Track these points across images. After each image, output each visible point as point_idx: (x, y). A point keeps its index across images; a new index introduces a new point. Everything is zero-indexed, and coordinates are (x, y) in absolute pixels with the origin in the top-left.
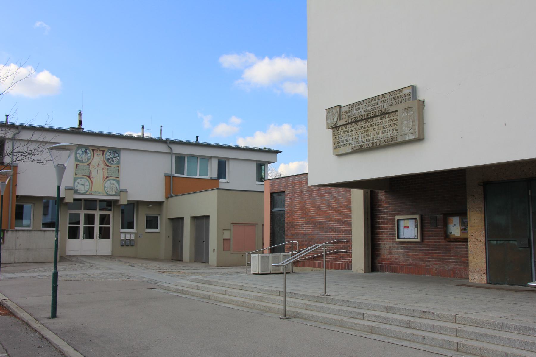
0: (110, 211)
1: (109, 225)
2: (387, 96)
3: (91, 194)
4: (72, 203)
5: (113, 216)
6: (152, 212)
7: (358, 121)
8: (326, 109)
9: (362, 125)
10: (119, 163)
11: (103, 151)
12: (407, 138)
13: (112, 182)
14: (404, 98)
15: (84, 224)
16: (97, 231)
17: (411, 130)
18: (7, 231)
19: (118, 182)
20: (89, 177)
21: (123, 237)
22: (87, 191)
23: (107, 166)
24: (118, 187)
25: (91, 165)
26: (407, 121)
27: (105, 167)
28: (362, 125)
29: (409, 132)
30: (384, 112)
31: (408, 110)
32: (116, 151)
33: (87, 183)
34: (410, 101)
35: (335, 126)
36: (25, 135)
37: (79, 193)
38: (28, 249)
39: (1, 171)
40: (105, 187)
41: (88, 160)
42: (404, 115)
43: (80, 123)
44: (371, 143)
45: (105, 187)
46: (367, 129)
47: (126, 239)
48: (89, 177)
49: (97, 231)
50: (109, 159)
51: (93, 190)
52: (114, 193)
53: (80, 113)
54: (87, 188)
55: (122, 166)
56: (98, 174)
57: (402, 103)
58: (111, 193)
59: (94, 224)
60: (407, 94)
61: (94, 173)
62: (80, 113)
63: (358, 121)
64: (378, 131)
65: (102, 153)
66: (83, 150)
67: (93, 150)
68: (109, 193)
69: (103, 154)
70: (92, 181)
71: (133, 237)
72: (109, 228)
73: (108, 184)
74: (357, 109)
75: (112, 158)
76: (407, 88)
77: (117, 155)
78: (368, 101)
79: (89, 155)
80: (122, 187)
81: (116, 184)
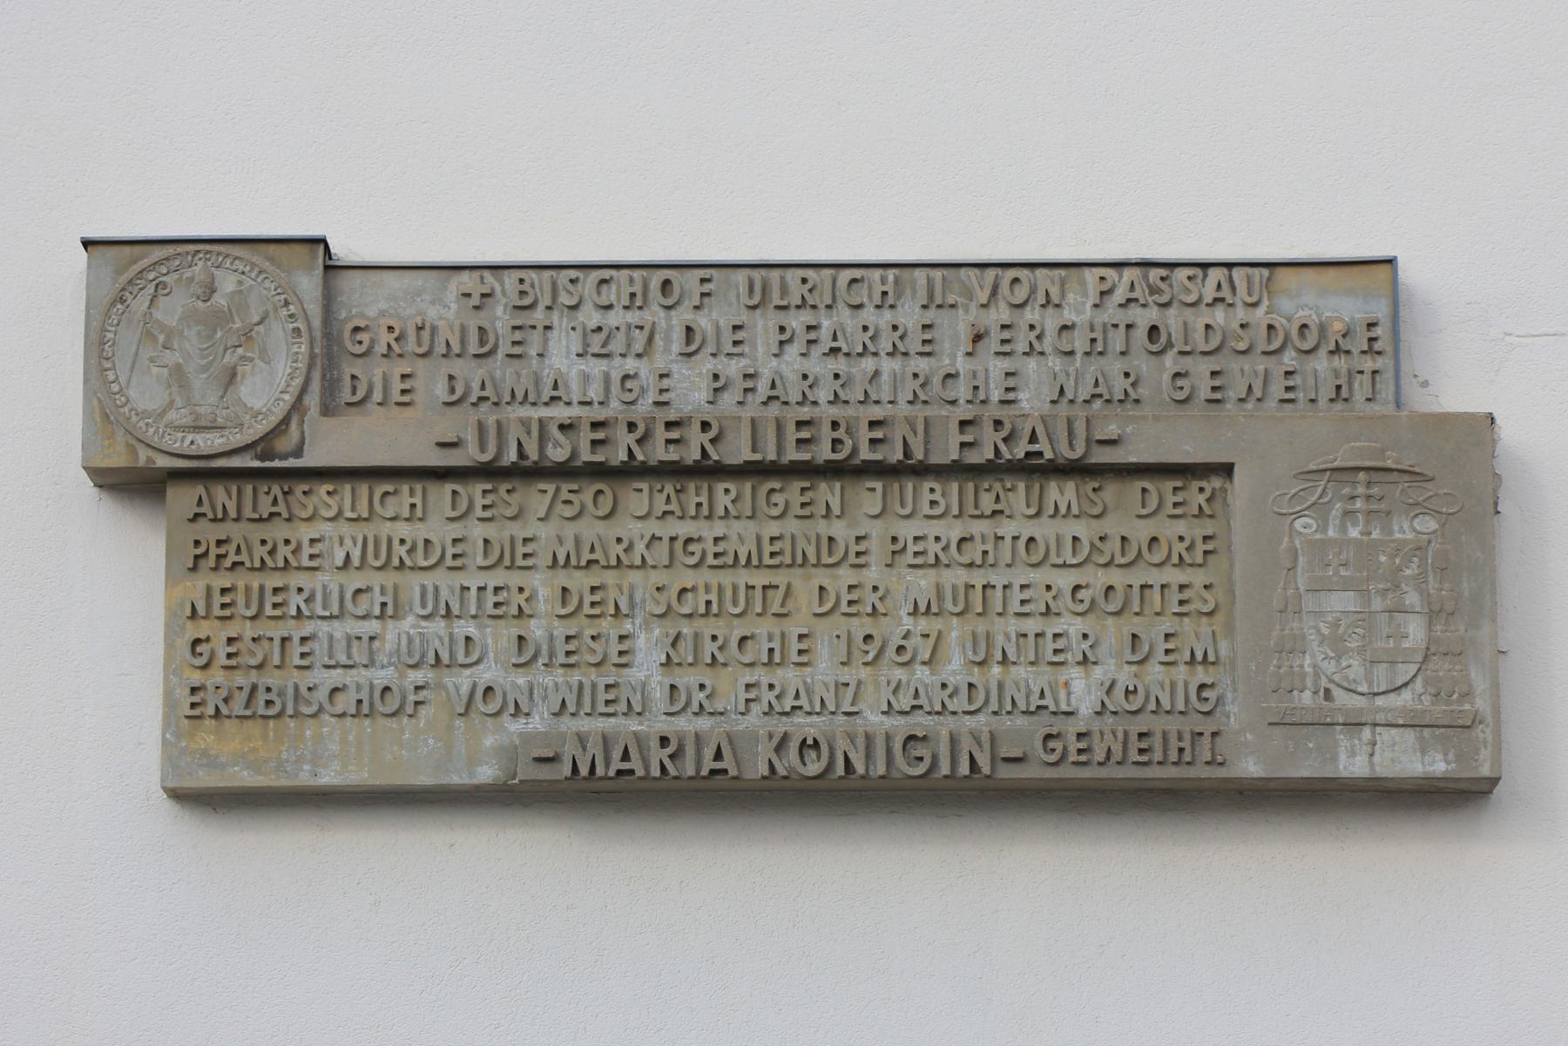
0: (669, 420)
2: (1063, 295)
7: (630, 471)
8: (87, 244)
9: (684, 529)
12: (1352, 763)
14: (1289, 359)
17: (1407, 695)
26: (1364, 594)
28: (684, 529)
29: (1380, 701)
30: (1043, 445)
31: (1375, 490)
34: (1376, 408)
35: (256, 464)
42: (1323, 528)
44: (605, 739)
46: (743, 577)
57: (1271, 404)
60: (1338, 326)
63: (630, 471)
64: (933, 625)
74: (596, 344)
76: (1332, 272)
78: (86, 381)
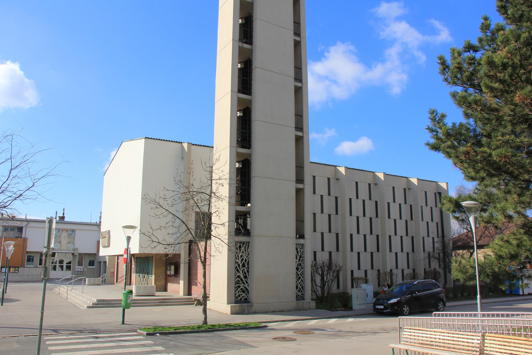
1: (71, 264)
3: (61, 250)
4: (174, 267)
5: (73, 262)
6: (92, 259)
10: (75, 236)
11: (67, 231)
13: (71, 244)
15: (63, 265)
16: (65, 267)
18: (20, 267)
19: (74, 245)
20: (60, 242)
21: (77, 270)
22: (59, 249)
23: (69, 237)
24: (74, 247)
25: (61, 237)
27: (68, 238)
32: (73, 231)
33: (59, 245)
36: (31, 224)
37: (55, 250)
38: (28, 275)
39: (531, 113)
40: (67, 247)
41: (60, 235)
43: (64, 214)
45: (67, 247)
47: (79, 271)
48: (60, 242)
49: (65, 267)
50: (70, 234)
51: (62, 248)
52: (72, 250)
53: (64, 210)
54: (59, 248)
55: (76, 237)
56: (64, 241)
58: (70, 250)
59: (67, 266)
61: (62, 241)
62: (64, 210)
65: (66, 231)
66: (58, 230)
67: (62, 230)
68: (69, 250)
69: (67, 232)
70: (61, 245)
71: (82, 270)
72: (71, 266)
73: (69, 246)
75: (71, 234)
77: (74, 232)
79: (60, 233)
80: (76, 247)
81: (73, 246)
